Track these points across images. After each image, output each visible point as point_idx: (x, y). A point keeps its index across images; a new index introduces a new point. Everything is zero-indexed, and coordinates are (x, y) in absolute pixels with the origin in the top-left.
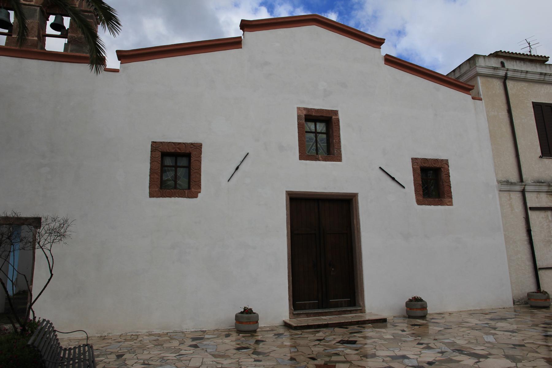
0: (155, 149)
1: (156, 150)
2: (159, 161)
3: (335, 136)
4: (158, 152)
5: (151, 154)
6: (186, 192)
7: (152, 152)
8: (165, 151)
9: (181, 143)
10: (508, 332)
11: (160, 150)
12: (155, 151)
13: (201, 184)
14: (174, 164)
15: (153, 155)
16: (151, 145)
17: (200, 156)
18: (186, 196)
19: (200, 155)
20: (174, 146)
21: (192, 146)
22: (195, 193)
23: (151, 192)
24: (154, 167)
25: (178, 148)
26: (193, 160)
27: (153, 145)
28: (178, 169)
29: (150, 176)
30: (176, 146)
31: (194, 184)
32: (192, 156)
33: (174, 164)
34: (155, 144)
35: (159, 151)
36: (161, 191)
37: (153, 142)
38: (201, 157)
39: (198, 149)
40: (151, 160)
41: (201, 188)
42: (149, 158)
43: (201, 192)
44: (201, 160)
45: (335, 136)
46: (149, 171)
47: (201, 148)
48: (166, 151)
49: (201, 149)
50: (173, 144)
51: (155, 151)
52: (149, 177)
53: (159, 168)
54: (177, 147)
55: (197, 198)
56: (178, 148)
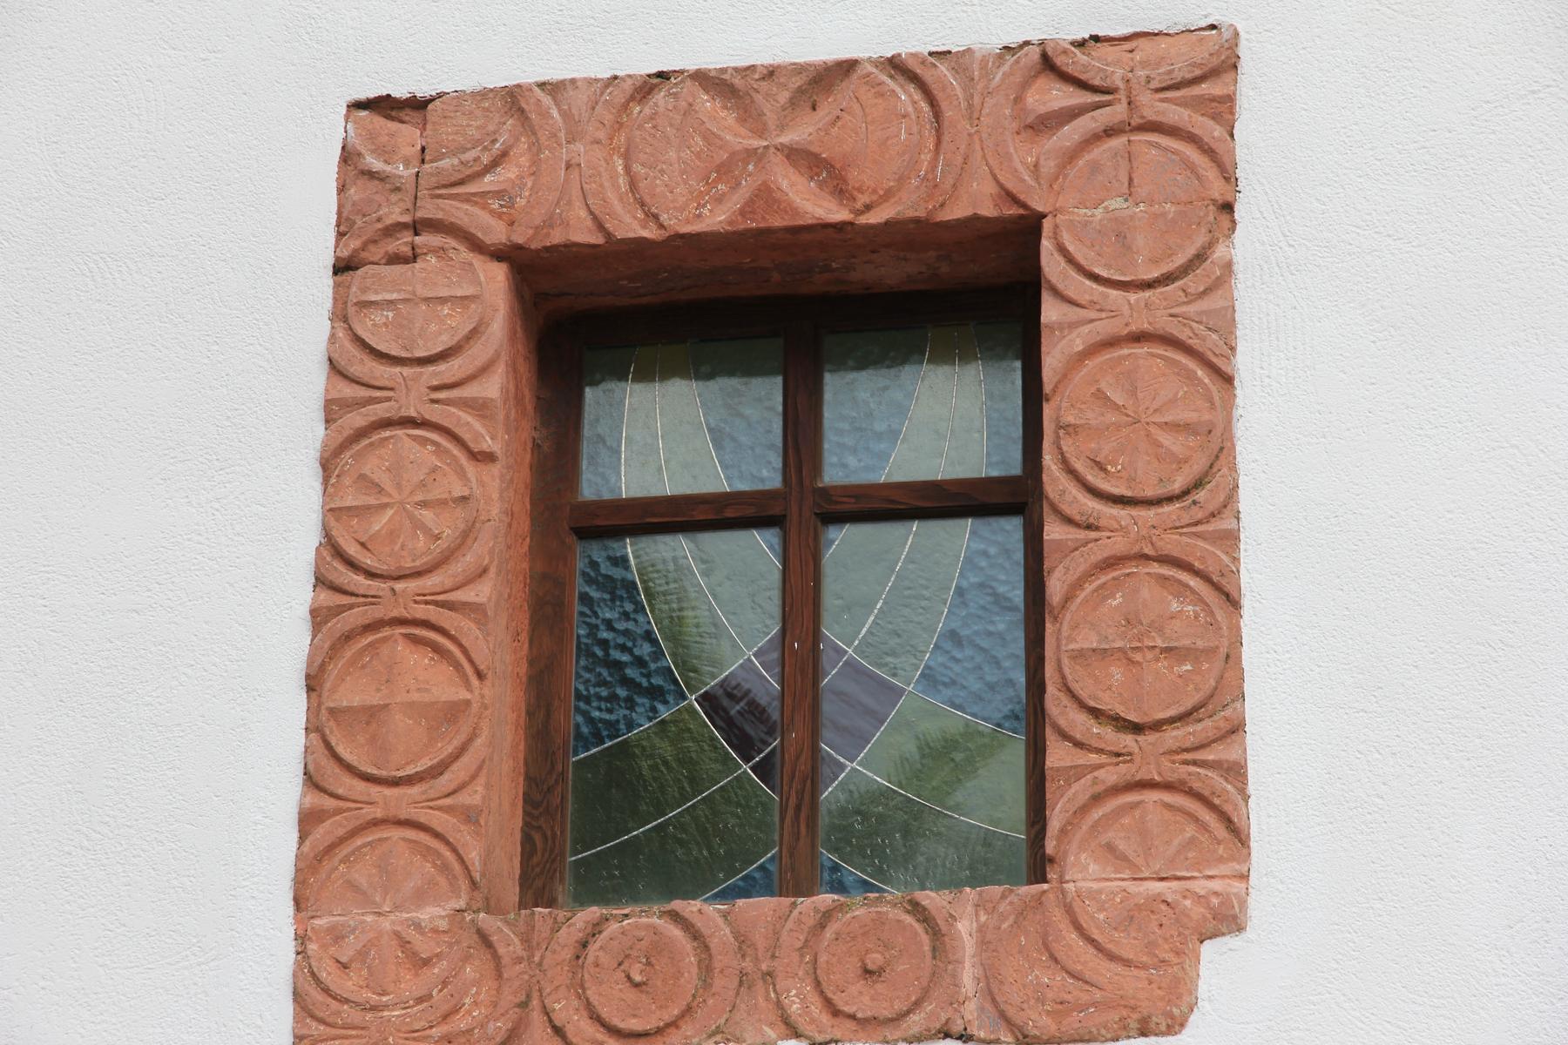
0: (395, 213)
1: (416, 227)
2: (480, 408)
3: (598, 142)
4: (465, 254)
5: (340, 315)
6: (965, 928)
7: (380, 281)
8: (583, 234)
9: (847, 67)
10: (1041, 660)
11: (497, 233)
12: (401, 243)
13: (1236, 772)
14: (765, 473)
15: (372, 327)
16: (348, 156)
17: (1200, 257)
18: (956, 1002)
19: (1200, 240)
20: (733, 133)
21: (1060, 96)
22: (1126, 945)
23: (328, 973)
24: (379, 523)
25: (807, 160)
26: (1077, 341)
27: (376, 164)
28: (841, 541)
29: (313, 684)
30: (761, 132)
31: (1111, 775)
32: (1051, 264)
33: (765, 473)
34: (407, 135)
35: (477, 246)
36: (509, 943)
37: (383, 106)
38: (1228, 266)
39: (1173, 131)
40: (332, 410)
41: (1238, 834)
42: (314, 383)
43: (1260, 906)
44: (1225, 325)
45: (598, 142)
46: (301, 595)
47: (1224, 109)
48: (597, 239)
49: (1210, 130)
50: (706, 103)
51: (401, 243)
52: (296, 706)
53: (466, 536)
54: (785, 139)
55: (1175, 1025)
56: (807, 160)
